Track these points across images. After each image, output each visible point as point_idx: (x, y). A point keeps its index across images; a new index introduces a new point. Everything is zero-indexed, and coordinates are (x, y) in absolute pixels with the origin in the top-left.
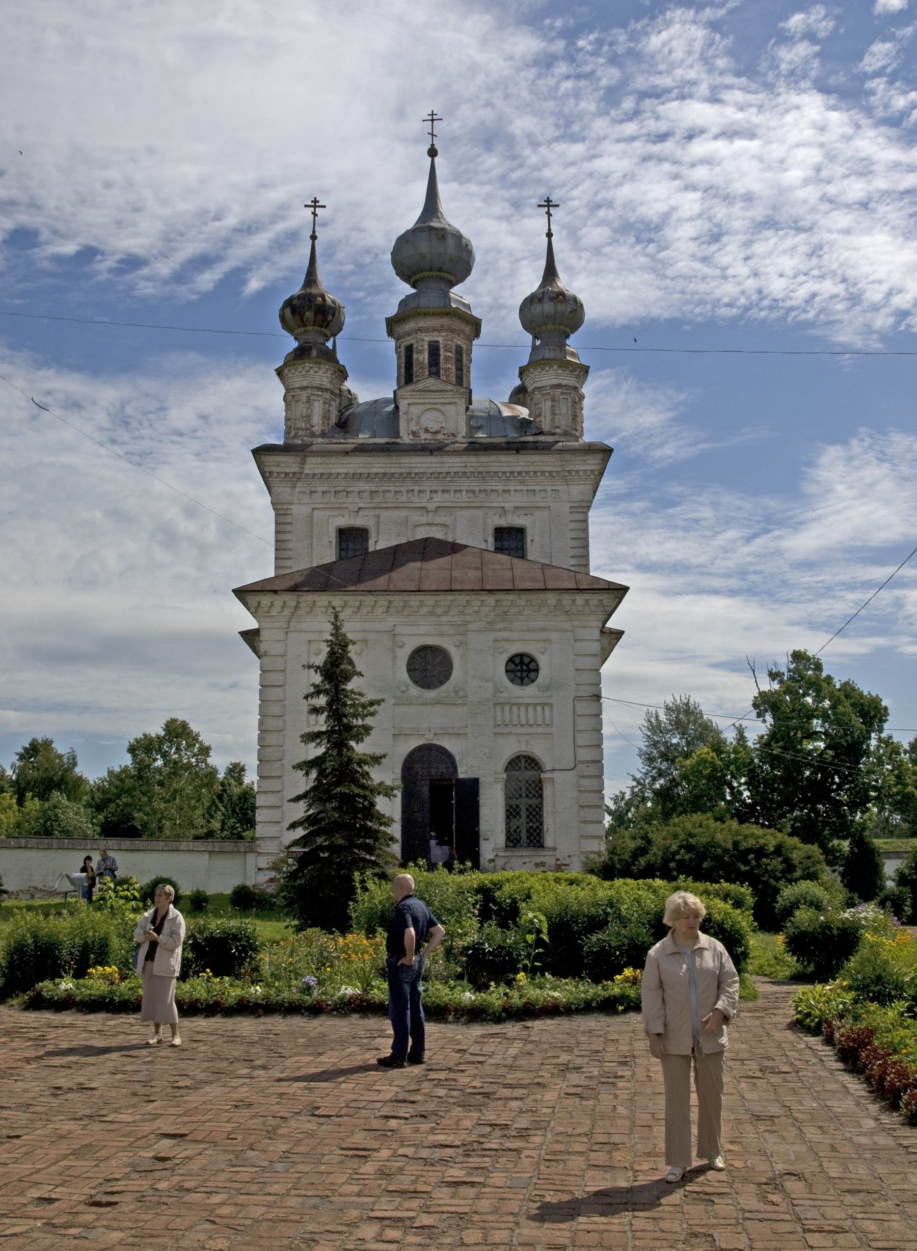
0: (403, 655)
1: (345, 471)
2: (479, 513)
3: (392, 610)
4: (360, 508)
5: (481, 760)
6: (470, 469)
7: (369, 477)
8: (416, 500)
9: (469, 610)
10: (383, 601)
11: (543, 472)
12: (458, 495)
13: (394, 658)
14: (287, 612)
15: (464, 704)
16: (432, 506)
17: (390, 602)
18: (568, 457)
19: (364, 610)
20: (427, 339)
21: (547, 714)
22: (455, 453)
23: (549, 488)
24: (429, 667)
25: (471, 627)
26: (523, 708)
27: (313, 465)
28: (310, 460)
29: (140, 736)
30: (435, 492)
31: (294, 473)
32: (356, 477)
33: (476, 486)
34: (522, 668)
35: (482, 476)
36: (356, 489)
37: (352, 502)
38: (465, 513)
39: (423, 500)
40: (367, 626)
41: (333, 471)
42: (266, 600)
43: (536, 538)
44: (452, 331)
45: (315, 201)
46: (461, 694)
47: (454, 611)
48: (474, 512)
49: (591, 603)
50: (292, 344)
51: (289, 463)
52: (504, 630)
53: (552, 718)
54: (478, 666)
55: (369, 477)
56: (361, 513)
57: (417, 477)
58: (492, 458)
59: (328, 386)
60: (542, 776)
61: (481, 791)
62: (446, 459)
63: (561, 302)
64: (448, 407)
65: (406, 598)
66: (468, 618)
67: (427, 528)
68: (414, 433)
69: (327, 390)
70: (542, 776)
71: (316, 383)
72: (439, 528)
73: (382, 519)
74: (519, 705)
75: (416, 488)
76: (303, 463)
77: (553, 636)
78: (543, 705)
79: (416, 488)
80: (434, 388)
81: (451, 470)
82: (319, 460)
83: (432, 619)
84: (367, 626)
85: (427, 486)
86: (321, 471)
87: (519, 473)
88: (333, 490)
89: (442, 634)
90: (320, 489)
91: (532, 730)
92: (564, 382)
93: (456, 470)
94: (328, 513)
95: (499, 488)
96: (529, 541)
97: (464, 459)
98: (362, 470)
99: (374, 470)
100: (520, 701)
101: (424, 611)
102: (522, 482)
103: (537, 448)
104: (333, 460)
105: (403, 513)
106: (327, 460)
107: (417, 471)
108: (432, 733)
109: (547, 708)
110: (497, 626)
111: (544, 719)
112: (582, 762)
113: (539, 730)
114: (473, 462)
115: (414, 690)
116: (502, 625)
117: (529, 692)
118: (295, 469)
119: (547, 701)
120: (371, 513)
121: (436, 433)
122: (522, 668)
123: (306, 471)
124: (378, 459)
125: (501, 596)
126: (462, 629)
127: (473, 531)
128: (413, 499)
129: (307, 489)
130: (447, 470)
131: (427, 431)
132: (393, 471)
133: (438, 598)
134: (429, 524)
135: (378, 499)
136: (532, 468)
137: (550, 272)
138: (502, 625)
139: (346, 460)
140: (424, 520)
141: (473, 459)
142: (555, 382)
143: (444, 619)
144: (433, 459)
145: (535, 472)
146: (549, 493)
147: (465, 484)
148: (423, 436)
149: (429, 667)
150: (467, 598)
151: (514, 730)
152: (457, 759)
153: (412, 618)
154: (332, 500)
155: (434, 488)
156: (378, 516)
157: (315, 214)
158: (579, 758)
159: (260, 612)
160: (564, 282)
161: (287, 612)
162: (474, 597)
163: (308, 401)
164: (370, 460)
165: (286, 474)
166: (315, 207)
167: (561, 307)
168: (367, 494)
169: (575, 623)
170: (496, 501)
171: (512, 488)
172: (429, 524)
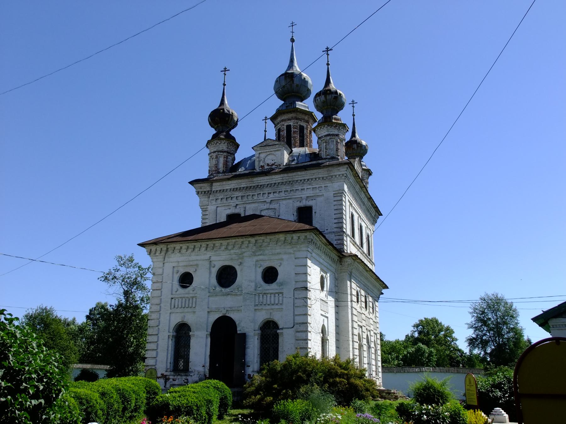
0: (215, 271)
1: (230, 188)
2: (291, 201)
3: (208, 249)
4: (237, 205)
5: (248, 323)
6: (285, 181)
7: (240, 189)
8: (265, 198)
9: (244, 246)
10: (204, 244)
11: (319, 178)
12: (275, 194)
13: (210, 273)
14: (163, 253)
15: (241, 295)
16: (268, 200)
17: (214, 244)
18: (330, 168)
19: (196, 250)
20: (286, 124)
21: (281, 298)
22: (276, 173)
23: (323, 186)
24: (226, 276)
25: (245, 254)
26: (269, 295)
27: (217, 186)
28: (214, 184)
29: (430, 317)
30: (270, 193)
31: (208, 191)
32: (235, 190)
33: (288, 188)
34: (270, 275)
35: (291, 183)
36: (235, 196)
37: (234, 202)
38: (284, 202)
39: (265, 198)
40: (198, 258)
41: (225, 188)
42: (153, 248)
43: (318, 211)
44: (297, 119)
45: (353, 101)
46: (240, 289)
47: (237, 247)
48: (288, 201)
49: (301, 238)
50: (213, 131)
51: (206, 187)
52: (261, 255)
53: (283, 301)
54: (249, 275)
55: (240, 189)
56: (238, 207)
57: (261, 187)
58: (294, 174)
59: (226, 149)
60: (278, 331)
61: (247, 340)
62: (273, 177)
63: (329, 94)
64: (277, 152)
65: (214, 242)
66: (243, 250)
67: (266, 211)
68: (262, 167)
69: (225, 152)
70: (278, 331)
71: (220, 149)
72: (272, 210)
73: (247, 209)
74: (268, 294)
75: (262, 192)
76: (212, 186)
77: (285, 257)
78: (279, 293)
79: (262, 192)
80: (271, 144)
81: (277, 182)
82: (218, 184)
83: (227, 251)
84: (198, 258)
85: (266, 190)
86: (220, 189)
87: (308, 180)
88: (225, 197)
89: (232, 259)
90: (220, 197)
91: (273, 307)
92: (332, 133)
93: (279, 181)
94: (223, 208)
95: (300, 188)
96: (313, 213)
97: (282, 175)
98: (237, 187)
99: (242, 186)
100: (267, 292)
101: (223, 248)
102: (310, 184)
103: (318, 166)
104: (224, 183)
105: (256, 205)
106: (221, 183)
107: (261, 184)
108: (225, 311)
109: (280, 295)
110: (257, 254)
111: (271, 301)
112: (297, 324)
113: (277, 307)
114: (286, 177)
115: (219, 288)
116: (259, 253)
117: (273, 287)
118: (208, 189)
119: (281, 291)
120: (243, 206)
121: (273, 165)
122: (270, 275)
123: (213, 190)
124: (243, 181)
125: (257, 238)
126: (241, 256)
127: (287, 211)
128: (260, 198)
129: (215, 198)
130: (274, 182)
131: (268, 165)
132: (250, 185)
133: (228, 241)
134: (267, 209)
135: (245, 199)
136: (314, 177)
137: (328, 82)
138: (259, 253)
139: (230, 182)
140: (265, 207)
141: (286, 175)
142: (327, 133)
143: (232, 251)
144: (268, 177)
145: (316, 179)
146: (323, 188)
147: (283, 188)
148: (266, 167)
149: (226, 276)
150: (242, 240)
151: (264, 307)
152: (237, 323)
153: (218, 252)
154: (225, 202)
155: (270, 192)
156: (245, 208)
157: (353, 107)
158: (296, 322)
159: (152, 254)
160: (333, 86)
161: (163, 253)
162: (245, 239)
163: (217, 157)
164: (240, 181)
165: (205, 192)
166: (353, 104)
167: (329, 97)
168: (240, 198)
169: (295, 249)
170: (298, 195)
171: (305, 187)
172: (267, 209)
